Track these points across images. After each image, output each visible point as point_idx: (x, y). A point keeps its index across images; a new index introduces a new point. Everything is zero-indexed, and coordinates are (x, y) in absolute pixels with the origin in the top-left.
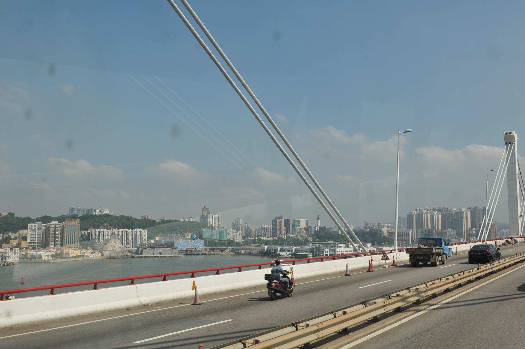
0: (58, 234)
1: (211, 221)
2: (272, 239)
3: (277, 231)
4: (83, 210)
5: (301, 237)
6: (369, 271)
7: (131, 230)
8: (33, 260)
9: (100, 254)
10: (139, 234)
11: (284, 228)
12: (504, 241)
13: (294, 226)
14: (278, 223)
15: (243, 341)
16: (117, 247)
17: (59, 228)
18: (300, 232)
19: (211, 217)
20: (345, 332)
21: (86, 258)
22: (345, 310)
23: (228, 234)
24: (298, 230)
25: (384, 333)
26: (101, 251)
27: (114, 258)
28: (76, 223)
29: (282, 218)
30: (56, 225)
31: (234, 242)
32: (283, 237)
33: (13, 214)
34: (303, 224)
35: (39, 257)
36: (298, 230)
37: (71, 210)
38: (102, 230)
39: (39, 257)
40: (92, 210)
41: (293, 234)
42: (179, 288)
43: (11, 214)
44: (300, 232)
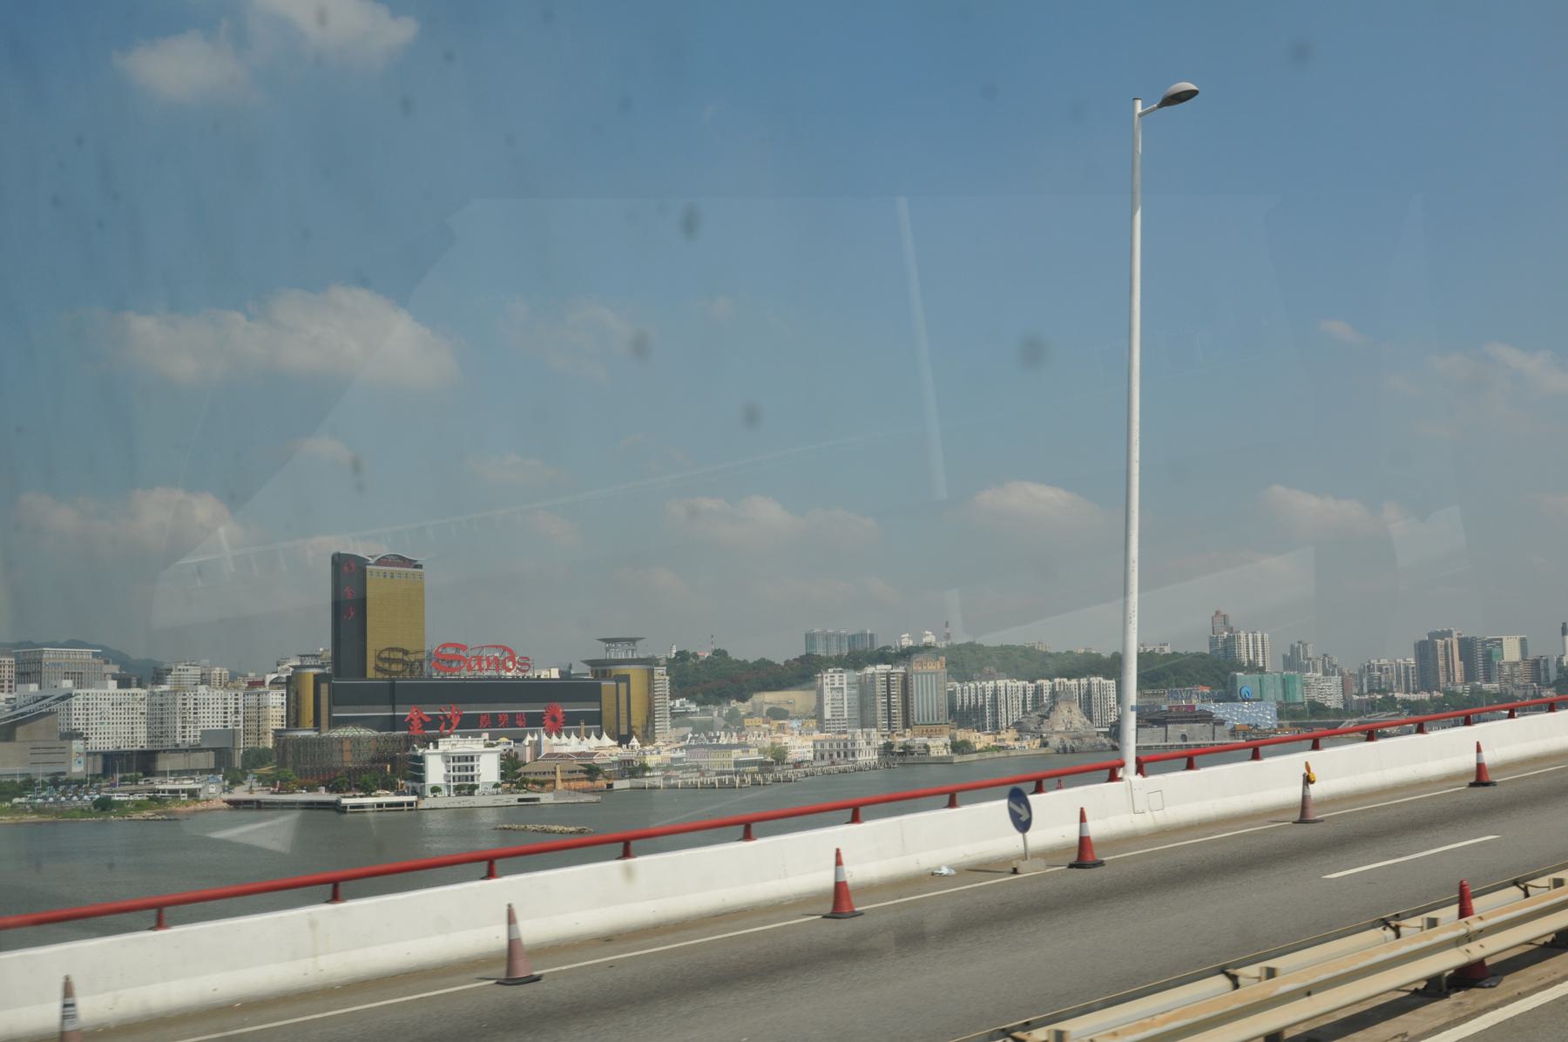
0: (896, 698)
1: (1243, 651)
2: (1425, 696)
3: (1437, 673)
4: (840, 638)
5: (1518, 687)
6: (1079, 864)
7: (1074, 682)
8: (909, 759)
9: (1038, 741)
10: (1095, 689)
11: (1458, 665)
12: (136, 816)
13: (1488, 657)
14: (1440, 651)
15: (1231, 971)
16: (1076, 724)
17: (897, 682)
18: (1512, 675)
19: (1243, 640)
20: (1470, 977)
21: (1013, 753)
22: (1270, 963)
23: (1307, 685)
24: (1507, 668)
25: (1511, 1019)
26: (1037, 734)
27: (1073, 751)
28: (937, 666)
29: (1449, 634)
30: (888, 675)
31: (1328, 709)
32: (1460, 689)
33: (724, 653)
34: (1511, 651)
35: (923, 750)
36: (1507, 668)
37: (810, 638)
38: (1001, 683)
39: (923, 750)
40: (863, 635)
41: (1488, 680)
42: (786, 867)
43: (720, 654)
44: (1512, 675)
